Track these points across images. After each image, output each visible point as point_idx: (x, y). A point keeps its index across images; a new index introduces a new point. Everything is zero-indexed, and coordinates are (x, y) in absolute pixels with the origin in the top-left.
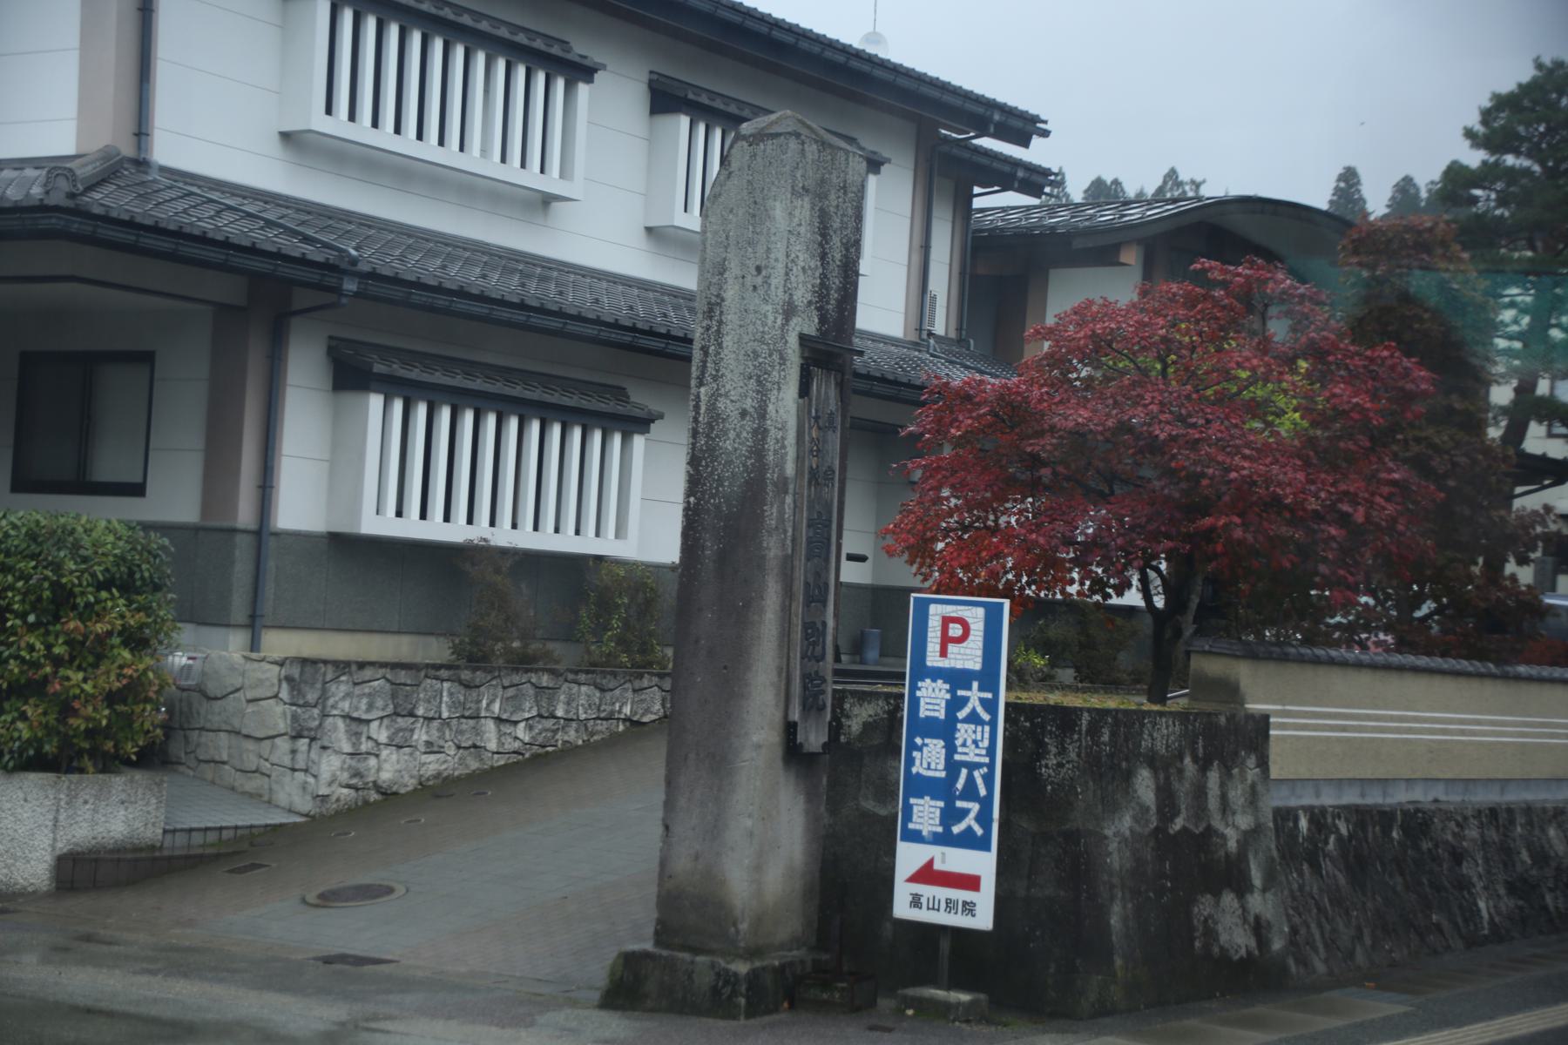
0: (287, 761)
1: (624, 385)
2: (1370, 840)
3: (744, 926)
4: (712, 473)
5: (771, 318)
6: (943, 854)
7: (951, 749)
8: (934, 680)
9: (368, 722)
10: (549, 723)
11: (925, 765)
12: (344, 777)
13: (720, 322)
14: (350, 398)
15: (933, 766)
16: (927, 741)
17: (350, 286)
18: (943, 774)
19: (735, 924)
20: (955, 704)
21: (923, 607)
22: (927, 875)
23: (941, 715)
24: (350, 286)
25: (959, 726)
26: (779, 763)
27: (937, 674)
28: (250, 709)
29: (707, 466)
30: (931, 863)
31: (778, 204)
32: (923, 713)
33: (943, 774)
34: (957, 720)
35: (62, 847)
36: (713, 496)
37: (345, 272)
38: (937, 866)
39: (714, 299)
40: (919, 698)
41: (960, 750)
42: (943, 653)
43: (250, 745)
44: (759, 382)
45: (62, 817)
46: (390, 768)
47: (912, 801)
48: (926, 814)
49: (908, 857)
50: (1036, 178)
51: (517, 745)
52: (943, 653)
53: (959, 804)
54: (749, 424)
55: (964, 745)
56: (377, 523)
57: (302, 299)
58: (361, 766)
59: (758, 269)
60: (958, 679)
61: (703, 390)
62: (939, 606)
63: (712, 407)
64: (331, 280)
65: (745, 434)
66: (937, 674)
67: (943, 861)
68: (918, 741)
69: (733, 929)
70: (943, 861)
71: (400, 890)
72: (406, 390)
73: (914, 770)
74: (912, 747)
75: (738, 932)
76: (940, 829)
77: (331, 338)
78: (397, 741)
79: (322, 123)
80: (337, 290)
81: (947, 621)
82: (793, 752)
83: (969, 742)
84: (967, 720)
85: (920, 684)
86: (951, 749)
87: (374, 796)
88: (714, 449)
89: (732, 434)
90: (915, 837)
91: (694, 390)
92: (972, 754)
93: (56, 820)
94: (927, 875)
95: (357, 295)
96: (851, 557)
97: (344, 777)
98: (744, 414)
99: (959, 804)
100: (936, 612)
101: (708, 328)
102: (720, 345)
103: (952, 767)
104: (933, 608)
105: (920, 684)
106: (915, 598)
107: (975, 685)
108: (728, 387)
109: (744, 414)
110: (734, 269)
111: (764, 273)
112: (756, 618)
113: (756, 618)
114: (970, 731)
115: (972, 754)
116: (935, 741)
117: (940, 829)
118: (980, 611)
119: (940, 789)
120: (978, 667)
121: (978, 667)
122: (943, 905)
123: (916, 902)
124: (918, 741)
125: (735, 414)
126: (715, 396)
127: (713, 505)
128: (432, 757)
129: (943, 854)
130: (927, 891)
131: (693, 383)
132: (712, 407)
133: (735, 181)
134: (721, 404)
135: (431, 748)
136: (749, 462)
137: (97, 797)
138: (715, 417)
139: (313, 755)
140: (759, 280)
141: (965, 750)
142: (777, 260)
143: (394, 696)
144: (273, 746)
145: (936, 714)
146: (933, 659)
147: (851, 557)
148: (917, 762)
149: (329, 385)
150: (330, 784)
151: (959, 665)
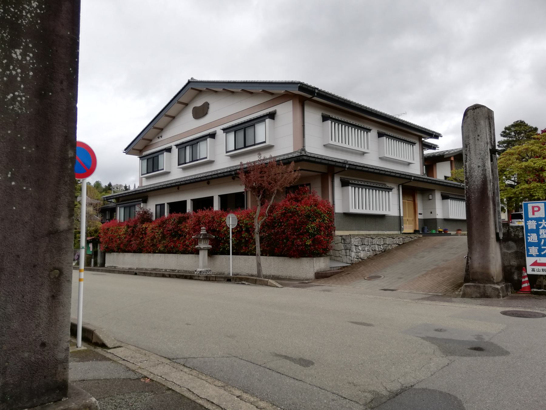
0: (345, 254)
1: (385, 183)
2: (270, 281)
3: (495, 278)
4: (472, 181)
5: (483, 145)
6: (540, 259)
7: (538, 235)
8: (531, 220)
9: (358, 246)
10: (386, 245)
11: (532, 240)
12: (355, 257)
13: (469, 148)
14: (345, 188)
15: (534, 240)
16: (531, 234)
17: (347, 166)
18: (537, 241)
19: (493, 278)
20: (538, 226)
21: (526, 205)
22: (535, 264)
23: (535, 228)
24: (347, 166)
25: (540, 230)
26: (496, 242)
27: (532, 219)
28: (336, 245)
29: (470, 179)
30: (536, 261)
31: (482, 121)
32: (529, 228)
33: (537, 241)
34: (540, 229)
35: (315, 271)
36: (473, 185)
37: (346, 164)
38: (538, 262)
39: (467, 144)
40: (528, 225)
41: (541, 235)
42: (533, 214)
43: (337, 252)
44: (482, 159)
45: (315, 265)
46: (362, 255)
47: (529, 248)
48: (533, 250)
49: (529, 261)
50: (435, 146)
51: (381, 249)
52: (533, 214)
53: (542, 247)
54: (481, 169)
55: (542, 234)
56: (352, 210)
57: (337, 170)
58: (358, 255)
59: (479, 136)
60: (539, 220)
61: (467, 163)
62: (531, 204)
63: (470, 166)
64: (344, 165)
65: (480, 171)
66: (532, 219)
67: (540, 261)
68: (529, 234)
69: (492, 279)
70: (540, 261)
71: (383, 277)
72: (355, 185)
73: (529, 241)
74: (527, 236)
75: (494, 279)
76: (538, 253)
77: (340, 178)
78: (363, 249)
79: (331, 142)
80: (345, 167)
81: (533, 207)
82: (498, 239)
83: (543, 233)
84: (542, 228)
85: (527, 222)
86: (538, 235)
87: (360, 260)
88: (472, 175)
89: (476, 171)
90: (532, 256)
91: (464, 163)
92: (545, 236)
93: (314, 266)
94: (535, 264)
95: (348, 168)
96: (420, 214)
97: (355, 257)
98: (479, 167)
99: (542, 247)
100: (530, 206)
101: (466, 150)
102: (470, 153)
103: (539, 240)
104: (529, 205)
105: (527, 222)
106: (524, 203)
107: (544, 220)
108: (474, 161)
109: (479, 167)
110: (471, 137)
111: (480, 136)
112: (489, 210)
113: (489, 210)
114: (543, 231)
115: (545, 236)
116: (534, 234)
117: (538, 253)
118: (543, 204)
119: (537, 244)
120: (544, 216)
121: (544, 216)
122: (541, 270)
123: (533, 270)
124: (529, 234)
125: (477, 167)
126: (470, 164)
127: (473, 187)
128: (368, 252)
129: (540, 259)
130: (536, 268)
131: (464, 162)
132: (470, 166)
133: (469, 119)
134: (472, 165)
135: (368, 251)
136: (482, 177)
137: (319, 261)
138: (471, 168)
139: (350, 252)
140: (479, 138)
141: (542, 235)
142: (483, 133)
143: (362, 241)
144: (342, 252)
145: (533, 228)
146: (530, 215)
147: (420, 214)
148: (529, 239)
149: (341, 186)
150: (353, 258)
151: (538, 216)
